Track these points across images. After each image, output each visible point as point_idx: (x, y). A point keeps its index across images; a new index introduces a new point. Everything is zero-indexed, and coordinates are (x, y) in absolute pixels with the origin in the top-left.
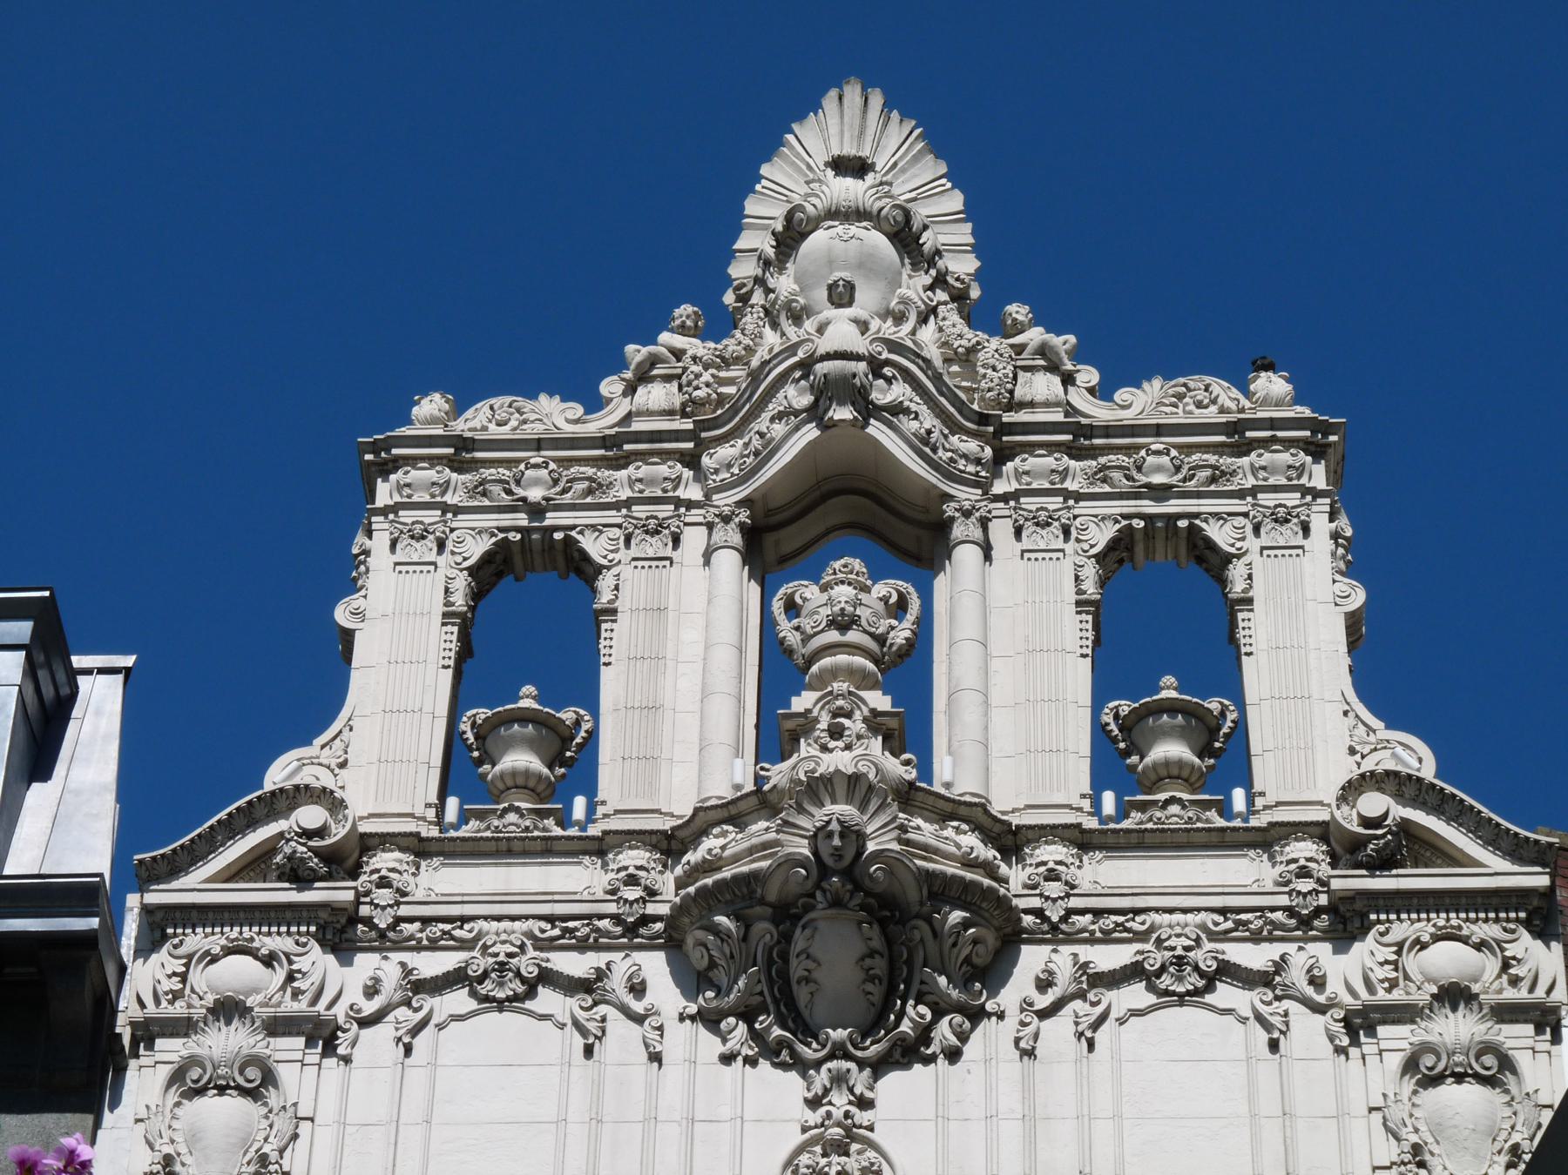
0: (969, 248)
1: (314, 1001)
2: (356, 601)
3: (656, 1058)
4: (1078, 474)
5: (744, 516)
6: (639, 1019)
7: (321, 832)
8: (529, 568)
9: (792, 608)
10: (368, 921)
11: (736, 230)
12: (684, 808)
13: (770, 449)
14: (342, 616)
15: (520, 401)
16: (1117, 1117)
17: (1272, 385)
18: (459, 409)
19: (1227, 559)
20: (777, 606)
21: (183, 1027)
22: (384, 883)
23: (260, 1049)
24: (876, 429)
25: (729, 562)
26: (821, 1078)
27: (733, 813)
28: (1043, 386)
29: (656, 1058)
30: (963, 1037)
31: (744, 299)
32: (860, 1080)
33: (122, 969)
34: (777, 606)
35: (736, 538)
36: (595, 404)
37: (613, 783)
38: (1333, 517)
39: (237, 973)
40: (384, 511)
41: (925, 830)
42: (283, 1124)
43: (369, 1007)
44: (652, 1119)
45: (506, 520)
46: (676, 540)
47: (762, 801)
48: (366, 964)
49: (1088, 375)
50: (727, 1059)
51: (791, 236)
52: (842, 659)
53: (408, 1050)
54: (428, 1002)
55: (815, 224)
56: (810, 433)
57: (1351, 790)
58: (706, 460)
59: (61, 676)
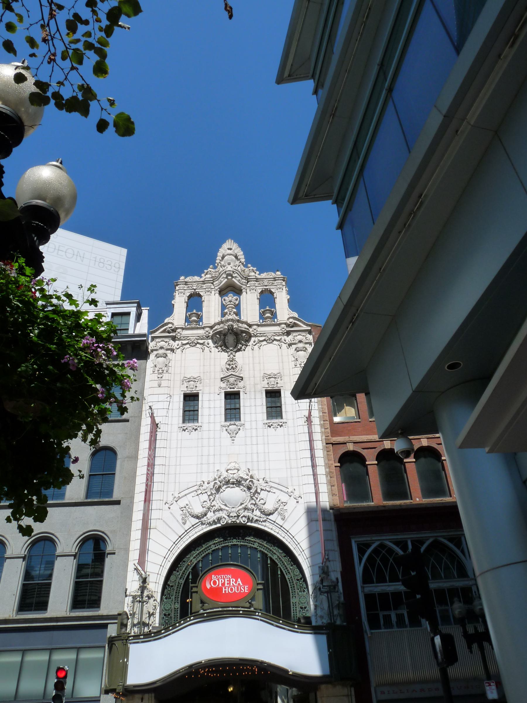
1: (171, 347)
2: (174, 301)
5: (219, 290)
6: (208, 347)
7: (171, 327)
8: (194, 296)
9: (224, 300)
13: (221, 282)
17: (278, 273)
20: (223, 300)
21: (156, 350)
22: (179, 333)
24: (233, 279)
25: (217, 295)
26: (229, 353)
27: (219, 324)
28: (253, 274)
30: (245, 348)
32: (234, 353)
34: (223, 300)
35: (218, 292)
36: (201, 277)
38: (286, 288)
39: (162, 344)
41: (240, 325)
42: (168, 361)
43: (178, 347)
45: (191, 291)
46: (211, 292)
47: (222, 322)
49: (258, 272)
51: (223, 257)
52: (230, 306)
53: (182, 352)
55: (226, 256)
56: (226, 280)
58: (214, 283)
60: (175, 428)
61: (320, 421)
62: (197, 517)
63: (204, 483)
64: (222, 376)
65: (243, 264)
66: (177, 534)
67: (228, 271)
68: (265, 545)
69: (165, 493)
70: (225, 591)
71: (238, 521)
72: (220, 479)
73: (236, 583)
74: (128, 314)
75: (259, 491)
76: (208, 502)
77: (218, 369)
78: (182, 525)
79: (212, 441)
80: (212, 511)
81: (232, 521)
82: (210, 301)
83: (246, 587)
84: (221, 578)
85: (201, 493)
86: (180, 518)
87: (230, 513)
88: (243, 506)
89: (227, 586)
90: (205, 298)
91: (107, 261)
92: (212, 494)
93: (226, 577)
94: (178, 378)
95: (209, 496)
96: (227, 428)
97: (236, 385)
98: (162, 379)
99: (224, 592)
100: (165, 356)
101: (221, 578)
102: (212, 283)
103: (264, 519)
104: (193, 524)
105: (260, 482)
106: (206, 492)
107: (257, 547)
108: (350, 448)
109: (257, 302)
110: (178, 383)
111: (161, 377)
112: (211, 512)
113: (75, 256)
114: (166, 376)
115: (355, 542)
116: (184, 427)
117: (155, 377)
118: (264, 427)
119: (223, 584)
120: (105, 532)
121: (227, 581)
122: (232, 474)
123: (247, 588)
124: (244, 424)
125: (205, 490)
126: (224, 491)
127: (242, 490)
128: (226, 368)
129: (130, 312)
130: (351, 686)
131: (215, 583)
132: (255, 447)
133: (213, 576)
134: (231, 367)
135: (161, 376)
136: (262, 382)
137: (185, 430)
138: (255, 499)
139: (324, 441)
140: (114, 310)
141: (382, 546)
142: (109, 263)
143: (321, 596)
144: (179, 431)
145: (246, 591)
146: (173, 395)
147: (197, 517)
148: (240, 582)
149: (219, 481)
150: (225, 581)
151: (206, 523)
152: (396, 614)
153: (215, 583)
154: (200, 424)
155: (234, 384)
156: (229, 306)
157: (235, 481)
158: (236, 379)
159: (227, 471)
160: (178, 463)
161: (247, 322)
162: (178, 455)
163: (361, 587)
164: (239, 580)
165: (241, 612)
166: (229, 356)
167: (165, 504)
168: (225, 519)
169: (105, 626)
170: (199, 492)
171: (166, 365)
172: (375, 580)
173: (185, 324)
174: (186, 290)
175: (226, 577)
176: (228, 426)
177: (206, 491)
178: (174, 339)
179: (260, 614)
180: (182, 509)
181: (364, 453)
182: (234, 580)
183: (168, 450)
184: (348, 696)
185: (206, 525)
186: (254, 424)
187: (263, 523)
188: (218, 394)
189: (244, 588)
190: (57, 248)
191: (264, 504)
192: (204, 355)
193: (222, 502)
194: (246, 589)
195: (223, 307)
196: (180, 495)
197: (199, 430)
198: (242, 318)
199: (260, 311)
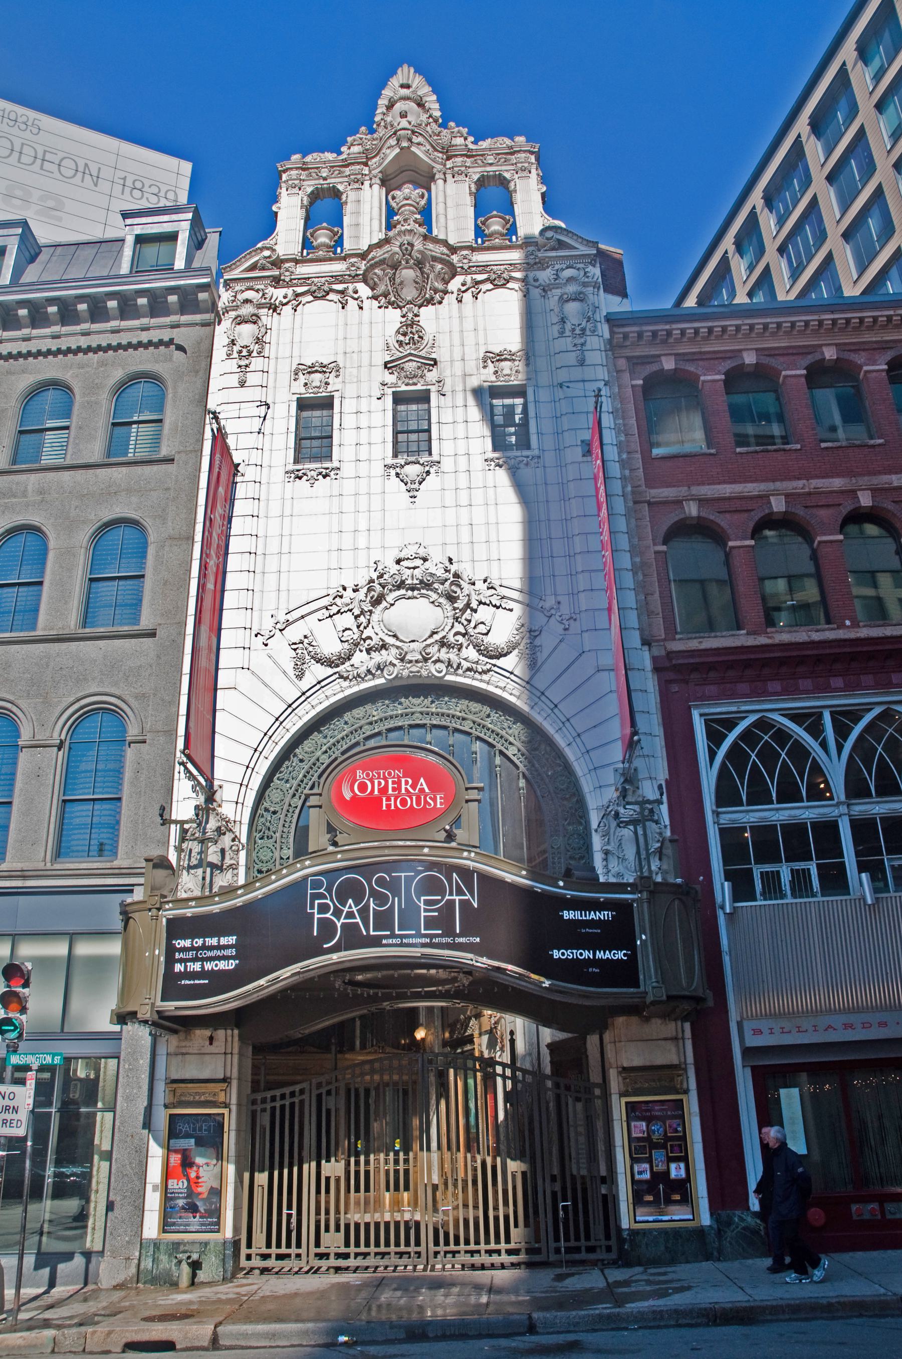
0: (396, 899)
1: (270, 299)
2: (278, 205)
3: (361, 308)
4: (469, 162)
5: (380, 175)
6: (356, 299)
7: (269, 257)
8: (324, 197)
9: (394, 198)
10: (284, 281)
11: (376, 109)
12: (365, 248)
13: (386, 156)
14: (274, 208)
15: (320, 154)
16: (484, 316)
17: (521, 139)
18: (304, 157)
19: (509, 182)
20: (390, 197)
21: (236, 308)
22: (287, 270)
23: (256, 312)
24: (413, 149)
25: (376, 187)
26: (405, 310)
27: (380, 245)
28: (459, 141)
29: (361, 308)
30: (443, 298)
31: (378, 125)
32: (416, 309)
33: (220, 297)
34: (390, 197)
35: (378, 182)
36: (340, 153)
37: (347, 244)
38: (537, 169)
39: (250, 295)
40: (285, 182)
41: (431, 246)
42: (263, 330)
43: (285, 301)
44: (360, 337)
45: (317, 182)
46: (362, 184)
47: (387, 241)
48: (282, 291)
49: (471, 139)
50: (380, 307)
51: (390, 107)
52: (407, 208)
53: (295, 310)
54: (300, 299)
55: (396, 102)
56: (397, 150)
57: (542, 232)
58: (369, 163)
59: (203, 233)
60: (278, 474)
61: (619, 453)
62: (329, 662)
63: (345, 589)
64: (388, 359)
65: (436, 121)
66: (283, 700)
67: (401, 130)
68: (490, 726)
69: (256, 614)
70: (388, 806)
71: (424, 673)
72: (382, 581)
73: (414, 786)
74: (172, 237)
75: (474, 605)
76: (355, 630)
77: (379, 345)
78: (296, 680)
79: (363, 499)
80: (364, 649)
81: (411, 672)
82: (359, 213)
83: (438, 797)
84: (379, 778)
85: (338, 612)
86: (289, 667)
87: (406, 653)
88: (437, 637)
89: (392, 795)
90: (350, 196)
91: (150, 187)
92: (362, 613)
93: (390, 774)
94: (286, 368)
95: (356, 617)
96: (398, 470)
97: (422, 377)
98: (248, 370)
99: (384, 808)
100: (254, 319)
101: (379, 778)
102: (366, 164)
103: (485, 668)
104: (320, 679)
105: (477, 587)
106: (351, 610)
107: (470, 730)
108: (690, 510)
109: (469, 201)
110: (285, 377)
111: (247, 366)
112: (361, 651)
113: (80, 175)
114: (257, 363)
115: (701, 715)
116: (298, 471)
117: (232, 365)
118: (487, 468)
119: (383, 791)
120: (124, 697)
121: (394, 783)
122: (409, 568)
123: (441, 798)
124: (439, 462)
125: (347, 605)
126: (392, 605)
127: (433, 602)
128: (397, 341)
129: (178, 232)
130: (684, 1019)
131: (363, 787)
132: (464, 511)
133: (359, 773)
134: (407, 338)
135: (247, 362)
136: (482, 370)
137: (300, 478)
138: (465, 623)
139: (630, 497)
140: (143, 229)
141: (763, 724)
142: (155, 190)
143: (619, 830)
144: (287, 480)
145: (438, 806)
146: (274, 403)
147: (329, 662)
148: (425, 786)
149: (380, 584)
150: (387, 782)
151: (350, 677)
152: (792, 870)
153: (363, 787)
154: (335, 464)
155: (415, 376)
156: (403, 209)
157: (418, 582)
158: (419, 364)
159: (398, 562)
160: (285, 550)
161: (446, 241)
162: (286, 532)
163: (713, 812)
164: (422, 780)
165: (426, 850)
166: (403, 316)
167: (256, 636)
168: (394, 665)
169: (132, 891)
170: (334, 609)
171: (258, 338)
172: (744, 798)
173: (302, 253)
174: (304, 180)
175: (390, 774)
176: (402, 467)
177: (350, 607)
178: (277, 282)
179: (473, 855)
180: (294, 647)
181: (724, 521)
182: (410, 781)
183: (262, 521)
184: (675, 1039)
185: (351, 680)
186: (463, 461)
187: (485, 677)
188: (378, 399)
189: (435, 800)
190: (40, 156)
191: (487, 634)
192: (346, 316)
193: (386, 631)
194: (438, 801)
195: (391, 212)
196: (292, 617)
197: (334, 477)
198: (435, 232)
199: (476, 220)
